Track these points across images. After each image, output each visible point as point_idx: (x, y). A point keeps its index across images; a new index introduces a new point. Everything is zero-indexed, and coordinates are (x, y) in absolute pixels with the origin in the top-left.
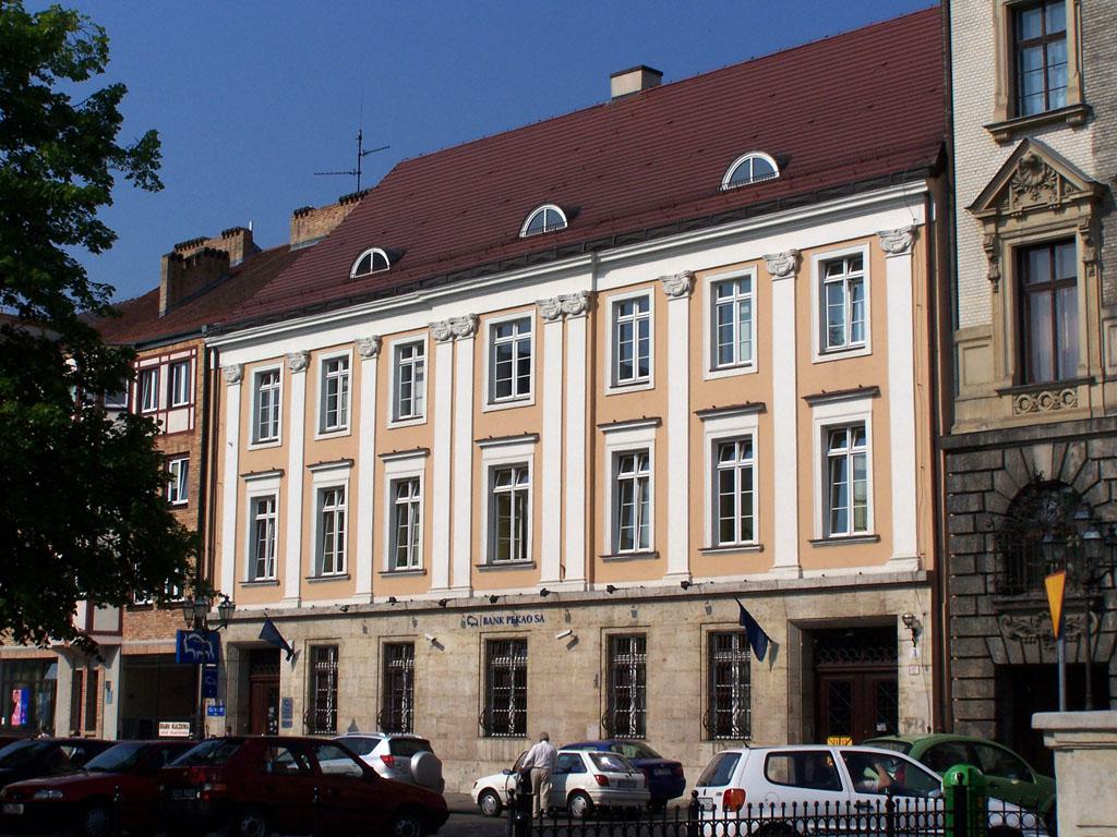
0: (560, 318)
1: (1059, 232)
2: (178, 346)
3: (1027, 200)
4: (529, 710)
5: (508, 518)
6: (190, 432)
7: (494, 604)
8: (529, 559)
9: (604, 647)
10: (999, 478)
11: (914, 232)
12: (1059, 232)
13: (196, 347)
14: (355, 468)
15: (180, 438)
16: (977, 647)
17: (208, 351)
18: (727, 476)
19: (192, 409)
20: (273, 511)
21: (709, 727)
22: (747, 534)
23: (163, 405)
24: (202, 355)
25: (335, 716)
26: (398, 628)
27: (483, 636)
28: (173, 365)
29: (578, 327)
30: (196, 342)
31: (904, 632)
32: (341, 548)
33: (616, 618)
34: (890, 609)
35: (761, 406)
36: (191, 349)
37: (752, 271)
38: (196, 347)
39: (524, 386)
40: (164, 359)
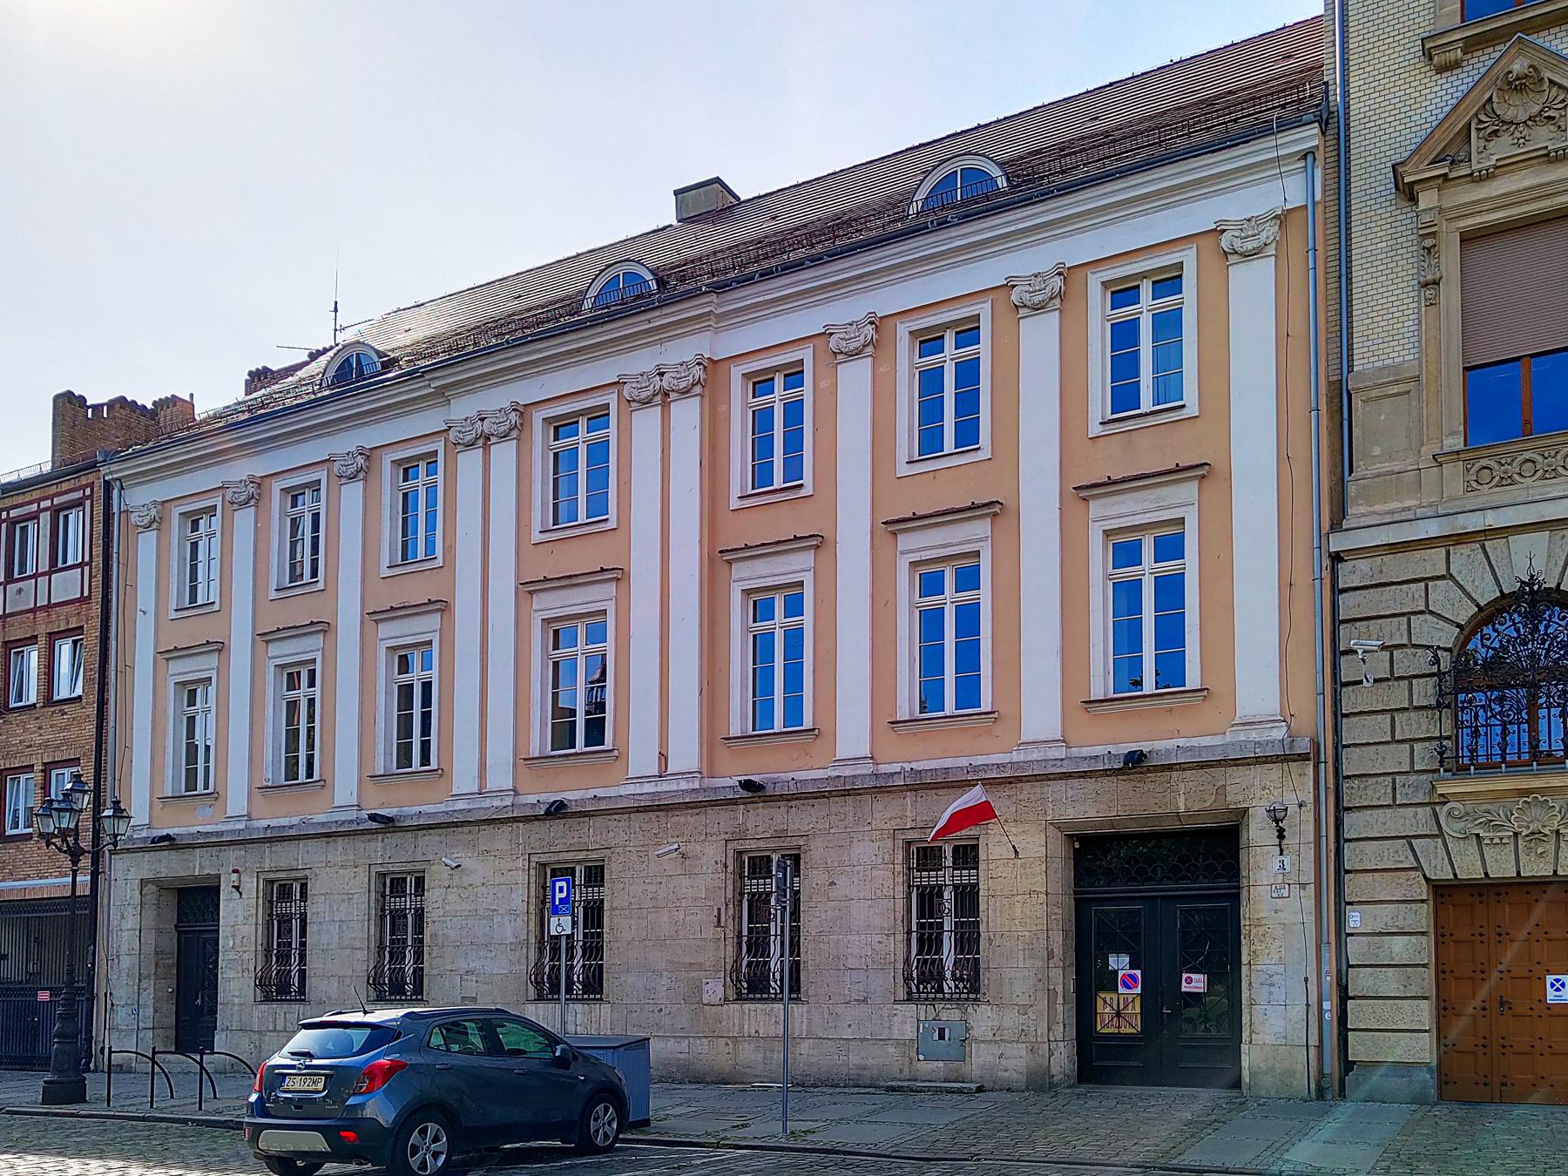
0: (480, 442)
1: (1478, 219)
2: (65, 487)
3: (1502, 148)
4: (802, 958)
5: (415, 718)
6: (83, 600)
7: (557, 810)
8: (434, 765)
9: (730, 869)
10: (1439, 590)
11: (1282, 219)
12: (1478, 219)
13: (91, 485)
14: (623, 584)
15: (66, 609)
16: (1397, 855)
17: (108, 486)
18: (293, 706)
19: (87, 569)
20: (312, 684)
21: (262, 983)
22: (425, 760)
23: (44, 566)
24: (99, 492)
25: (302, 974)
26: (760, 826)
27: (534, 859)
28: (56, 511)
29: (687, 414)
30: (91, 478)
31: (1258, 832)
32: (311, 746)
33: (750, 825)
34: (1234, 798)
35: (997, 509)
36: (83, 488)
37: (806, 354)
38: (91, 485)
39: (968, 435)
40: (46, 504)
